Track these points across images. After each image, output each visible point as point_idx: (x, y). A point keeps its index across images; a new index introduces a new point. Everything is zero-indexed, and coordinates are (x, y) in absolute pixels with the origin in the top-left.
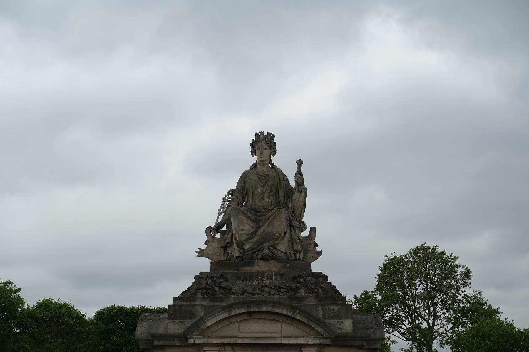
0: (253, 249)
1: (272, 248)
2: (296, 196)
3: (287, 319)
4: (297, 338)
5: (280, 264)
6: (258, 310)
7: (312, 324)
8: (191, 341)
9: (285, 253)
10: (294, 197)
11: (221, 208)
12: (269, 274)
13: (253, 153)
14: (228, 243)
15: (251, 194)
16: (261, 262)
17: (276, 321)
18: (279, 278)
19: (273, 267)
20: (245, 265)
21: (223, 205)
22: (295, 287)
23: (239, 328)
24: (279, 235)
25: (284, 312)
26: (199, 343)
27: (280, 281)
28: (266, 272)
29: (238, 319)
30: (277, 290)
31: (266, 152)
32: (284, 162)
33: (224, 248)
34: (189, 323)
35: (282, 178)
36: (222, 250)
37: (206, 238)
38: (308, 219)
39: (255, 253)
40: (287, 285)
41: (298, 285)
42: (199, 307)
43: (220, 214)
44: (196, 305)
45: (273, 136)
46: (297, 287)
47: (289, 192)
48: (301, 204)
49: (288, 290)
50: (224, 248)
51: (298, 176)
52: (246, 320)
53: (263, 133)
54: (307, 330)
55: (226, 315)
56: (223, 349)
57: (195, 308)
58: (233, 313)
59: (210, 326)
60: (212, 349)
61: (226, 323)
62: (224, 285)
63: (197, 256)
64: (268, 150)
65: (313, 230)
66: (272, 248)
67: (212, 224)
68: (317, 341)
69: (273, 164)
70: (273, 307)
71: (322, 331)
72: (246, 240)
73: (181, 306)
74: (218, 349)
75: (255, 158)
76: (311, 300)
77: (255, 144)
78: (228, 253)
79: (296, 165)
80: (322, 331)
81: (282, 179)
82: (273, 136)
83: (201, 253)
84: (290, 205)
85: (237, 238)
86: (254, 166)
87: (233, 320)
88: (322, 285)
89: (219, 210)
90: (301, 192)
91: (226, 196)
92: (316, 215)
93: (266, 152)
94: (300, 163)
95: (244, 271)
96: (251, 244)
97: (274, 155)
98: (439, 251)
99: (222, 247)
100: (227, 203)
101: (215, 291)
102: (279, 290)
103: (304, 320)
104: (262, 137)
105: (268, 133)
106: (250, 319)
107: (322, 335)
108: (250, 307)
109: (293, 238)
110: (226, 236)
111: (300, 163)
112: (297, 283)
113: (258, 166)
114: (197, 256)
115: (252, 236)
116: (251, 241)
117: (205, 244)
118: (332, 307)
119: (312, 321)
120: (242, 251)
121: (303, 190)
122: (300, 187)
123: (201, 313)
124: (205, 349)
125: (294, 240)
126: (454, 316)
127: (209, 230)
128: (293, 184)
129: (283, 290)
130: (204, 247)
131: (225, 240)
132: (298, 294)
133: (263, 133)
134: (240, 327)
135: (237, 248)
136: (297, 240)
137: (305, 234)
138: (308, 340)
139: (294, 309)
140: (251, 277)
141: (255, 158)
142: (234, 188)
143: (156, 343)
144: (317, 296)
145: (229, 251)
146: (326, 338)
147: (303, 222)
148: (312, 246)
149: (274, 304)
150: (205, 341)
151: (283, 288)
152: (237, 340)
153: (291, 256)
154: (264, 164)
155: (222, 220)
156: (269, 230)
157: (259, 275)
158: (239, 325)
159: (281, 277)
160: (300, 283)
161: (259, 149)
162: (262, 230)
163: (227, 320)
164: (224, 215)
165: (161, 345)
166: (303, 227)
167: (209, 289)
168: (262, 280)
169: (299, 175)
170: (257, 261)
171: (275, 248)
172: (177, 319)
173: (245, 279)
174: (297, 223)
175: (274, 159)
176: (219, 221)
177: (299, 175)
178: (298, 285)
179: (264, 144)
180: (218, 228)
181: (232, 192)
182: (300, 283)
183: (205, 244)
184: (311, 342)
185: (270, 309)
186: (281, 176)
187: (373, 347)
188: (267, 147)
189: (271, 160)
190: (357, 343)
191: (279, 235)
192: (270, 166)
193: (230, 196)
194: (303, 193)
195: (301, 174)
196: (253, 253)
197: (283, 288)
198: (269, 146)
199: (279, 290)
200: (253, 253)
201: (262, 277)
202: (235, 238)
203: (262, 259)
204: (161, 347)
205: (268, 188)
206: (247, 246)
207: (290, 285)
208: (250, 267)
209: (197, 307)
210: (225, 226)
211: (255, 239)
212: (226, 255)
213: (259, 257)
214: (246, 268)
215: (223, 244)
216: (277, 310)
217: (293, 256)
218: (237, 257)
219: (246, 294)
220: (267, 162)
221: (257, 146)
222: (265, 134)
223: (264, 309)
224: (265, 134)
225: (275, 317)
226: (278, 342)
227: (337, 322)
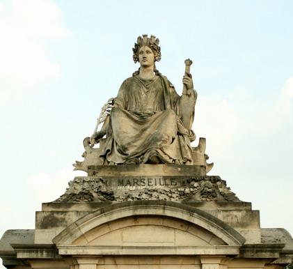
0: (137, 154)
1: (159, 151)
2: (184, 100)
3: (182, 226)
9: (174, 160)
10: (182, 103)
13: (136, 59)
14: (108, 151)
19: (160, 171)
22: (189, 192)
23: (122, 237)
24: (167, 137)
25: (179, 215)
26: (72, 254)
29: (122, 225)
30: (167, 195)
32: (170, 69)
33: (104, 157)
34: (60, 230)
35: (165, 85)
37: (84, 150)
38: (196, 127)
39: (140, 156)
41: (192, 190)
42: (73, 213)
45: (157, 41)
47: (177, 100)
48: (190, 110)
49: (181, 195)
53: (147, 36)
54: (207, 238)
57: (67, 214)
62: (104, 189)
65: (202, 140)
66: (159, 151)
68: (222, 251)
69: (158, 71)
73: (53, 212)
74: (96, 262)
75: (138, 65)
81: (167, 86)
85: (119, 144)
87: (115, 227)
88: (221, 190)
89: (99, 120)
90: (189, 96)
92: (207, 123)
94: (189, 63)
96: (135, 148)
99: (101, 156)
104: (145, 40)
111: (189, 63)
112: (190, 187)
115: (138, 137)
116: (135, 144)
124: (80, 261)
127: (87, 142)
128: (180, 90)
129: (174, 195)
130: (82, 160)
133: (147, 36)
134: (124, 235)
135: (119, 154)
136: (187, 148)
137: (195, 144)
138: (209, 250)
141: (138, 65)
142: (115, 96)
143: (20, 256)
144: (216, 201)
146: (233, 247)
149: (164, 204)
150: (80, 252)
151: (174, 193)
158: (122, 234)
165: (26, 259)
166: (191, 135)
167: (86, 194)
173: (129, 183)
174: (186, 130)
175: (159, 66)
177: (188, 87)
178: (192, 190)
179: (146, 48)
180: (98, 137)
183: (83, 156)
184: (213, 252)
185: (160, 212)
186: (167, 83)
187: (282, 262)
188: (150, 50)
190: (267, 255)
191: (167, 137)
194: (193, 96)
195: (189, 76)
196: (138, 157)
197: (174, 193)
198: (153, 49)
199: (170, 195)
200: (138, 157)
202: (117, 144)
203: (149, 162)
204: (26, 262)
206: (130, 151)
209: (70, 213)
213: (145, 160)
215: (103, 152)
224: (149, 37)
225: (166, 223)
226: (172, 252)
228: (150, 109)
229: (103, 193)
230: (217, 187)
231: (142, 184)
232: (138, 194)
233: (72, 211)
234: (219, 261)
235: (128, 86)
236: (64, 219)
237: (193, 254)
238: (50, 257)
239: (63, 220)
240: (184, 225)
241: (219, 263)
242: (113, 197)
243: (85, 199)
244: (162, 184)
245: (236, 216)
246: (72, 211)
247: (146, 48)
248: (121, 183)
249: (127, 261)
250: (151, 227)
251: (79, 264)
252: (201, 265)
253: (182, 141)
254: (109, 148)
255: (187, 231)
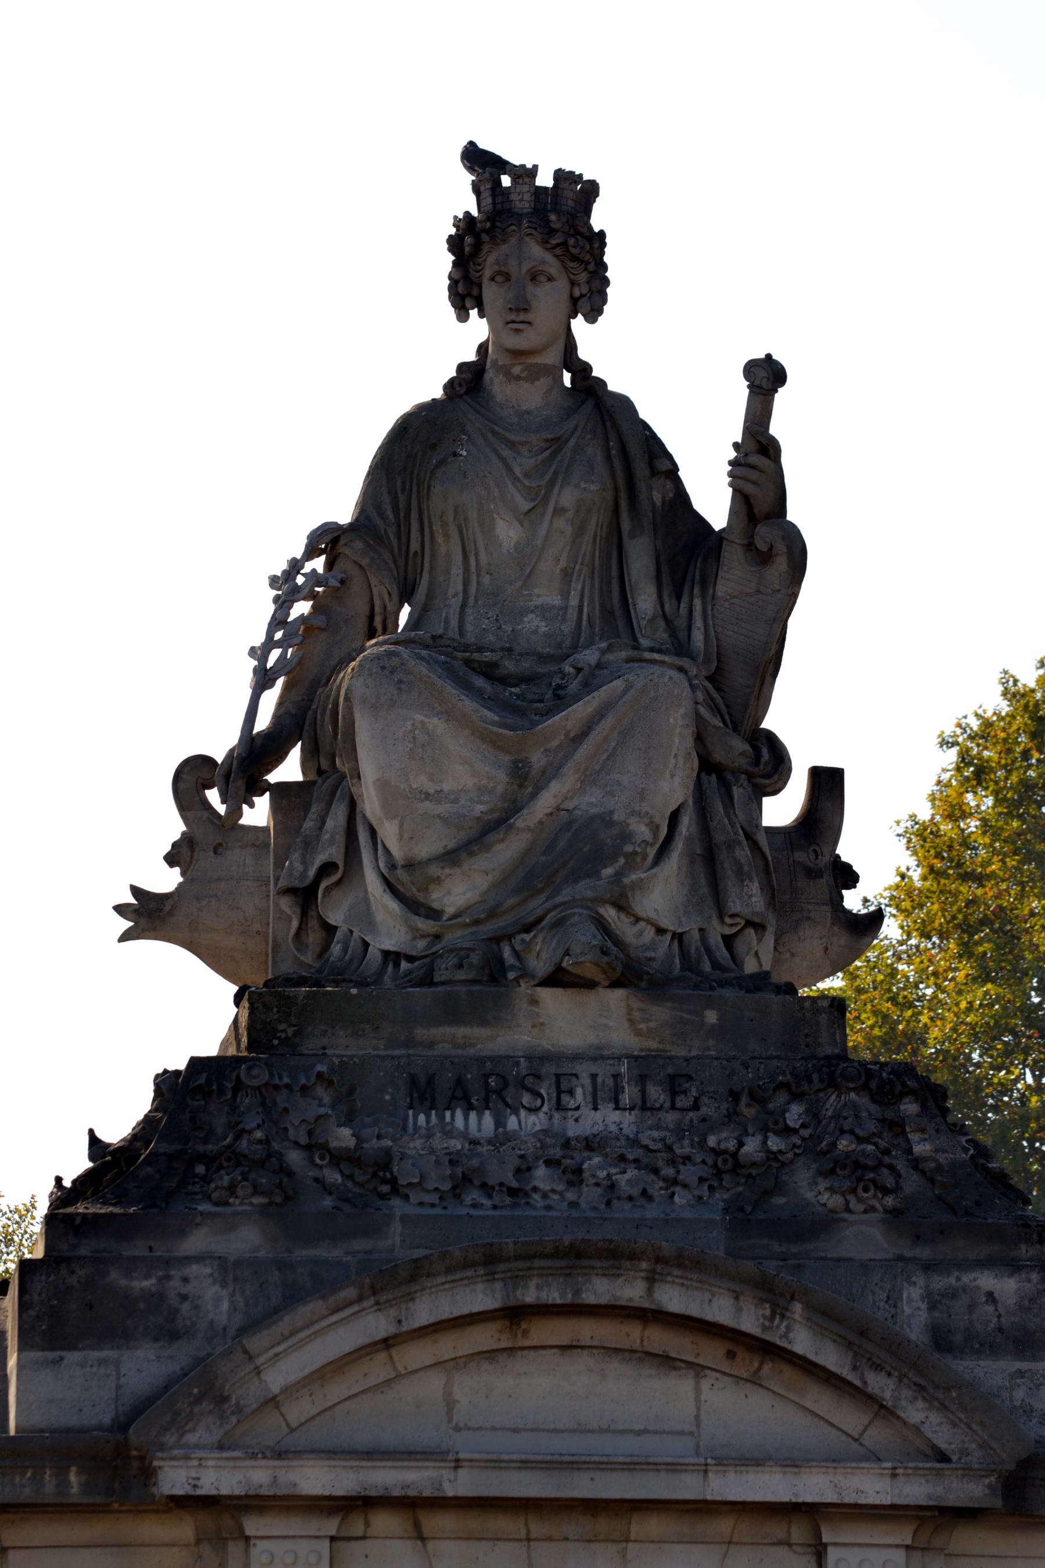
1: (609, 913)
4: (792, 1462)
5: (661, 1013)
6: (569, 1298)
7: (879, 1384)
8: (174, 1479)
9: (679, 937)
11: (269, 644)
12: (604, 1072)
13: (465, 295)
14: (328, 868)
15: (457, 558)
16: (546, 994)
17: (666, 1361)
18: (657, 1094)
20: (453, 1012)
21: (278, 621)
25: (720, 1309)
26: (225, 1491)
27: (671, 1118)
28: (577, 1057)
29: (448, 1346)
31: (548, 299)
34: (143, 1367)
36: (286, 904)
37: (174, 827)
40: (712, 1141)
41: (774, 1143)
43: (263, 680)
44: (189, 1260)
45: (592, 190)
46: (773, 1156)
49: (719, 1174)
50: (306, 896)
51: (756, 459)
52: (491, 1355)
53: (532, 172)
55: (376, 1324)
56: (357, 1527)
58: (425, 1310)
59: (286, 1390)
60: (295, 1525)
61: (378, 1369)
63: (125, 937)
64: (562, 285)
65: (827, 783)
66: (609, 913)
67: (220, 743)
68: (915, 1491)
69: (587, 368)
70: (651, 1280)
71: (940, 1431)
72: (451, 857)
74: (331, 1526)
75: (477, 329)
76: (864, 1237)
77: (477, 247)
78: (330, 930)
79: (741, 391)
80: (940, 1431)
81: (641, 470)
82: (592, 190)
83: (147, 915)
84: (698, 637)
86: (469, 381)
89: (259, 654)
91: (295, 566)
93: (548, 299)
94: (766, 377)
95: (443, 1049)
97: (593, 315)
98: (461, 216)
99: (290, 891)
100: (301, 608)
101: (291, 1174)
102: (670, 1172)
103: (831, 1357)
105: (560, 175)
106: (511, 1351)
107: (943, 1457)
108: (516, 1279)
109: (719, 838)
110: (309, 825)
111: (766, 377)
113: (497, 385)
114: (125, 937)
117: (171, 859)
118: (986, 1281)
119: (877, 1367)
120: (423, 924)
121: (781, 547)
122: (762, 529)
123: (216, 1302)
124: (252, 1525)
125: (723, 855)
126: (935, 939)
127: (192, 777)
128: (712, 501)
129: (689, 1173)
130: (166, 880)
131: (309, 846)
132: (781, 1200)
136: (743, 853)
137: (782, 809)
139: (775, 1297)
140: (494, 1085)
141: (477, 329)
142: (344, 514)
144: (895, 1213)
145: (335, 917)
146: (967, 1471)
147: (771, 739)
148: (825, 881)
150: (259, 1476)
152: (446, 1474)
153: (709, 951)
154: (535, 373)
155: (277, 717)
156: (591, 801)
157: (545, 1075)
159: (674, 1092)
160: (787, 1131)
161: (504, 276)
162: (546, 802)
163: (381, 1356)
164: (286, 688)
166: (771, 762)
168: (559, 1107)
169: (758, 459)
170: (525, 988)
171: (622, 906)
172: (73, 1348)
173: (461, 1096)
176: (263, 722)
177: (758, 459)
178: (774, 1143)
179: (530, 240)
181: (326, 540)
182: (787, 1131)
183: (171, 859)
184: (871, 1487)
185: (631, 1291)
186: (635, 449)
188: (552, 265)
189: (571, 345)
192: (567, 378)
193: (318, 564)
198: (565, 255)
199: (670, 1172)
201: (562, 1088)
202: (373, 833)
205: (560, 523)
206: (457, 892)
207: (731, 1145)
208: (484, 1022)
210: (295, 754)
211: (506, 851)
212: (314, 937)
213: (541, 966)
214: (462, 1032)
216: (674, 1298)
217: (722, 953)
218: (386, 954)
219: (472, 1195)
220: (553, 356)
221: (490, 261)
222: (545, 179)
223: (599, 1290)
225: (658, 1339)
227: (1020, 1373)
228: (543, 611)
229: (338, 1158)
230: (896, 1126)
231: (526, 1099)
232: (513, 1163)
233: (199, 1259)
234: (904, 1535)
235: (415, 452)
236: (161, 1296)
237: (785, 1497)
238: (90, 1500)
239: (156, 1299)
240: (741, 1353)
241: (908, 1541)
242: (393, 1182)
243: (256, 1191)
244: (626, 1099)
245: (990, 1296)
246: (199, 1259)
247: (530, 240)
248: (424, 1092)
249: (473, 1522)
250: (583, 1361)
251: (247, 1539)
252: (820, 1551)
253: (718, 806)
254: (331, 851)
255: (755, 1381)
